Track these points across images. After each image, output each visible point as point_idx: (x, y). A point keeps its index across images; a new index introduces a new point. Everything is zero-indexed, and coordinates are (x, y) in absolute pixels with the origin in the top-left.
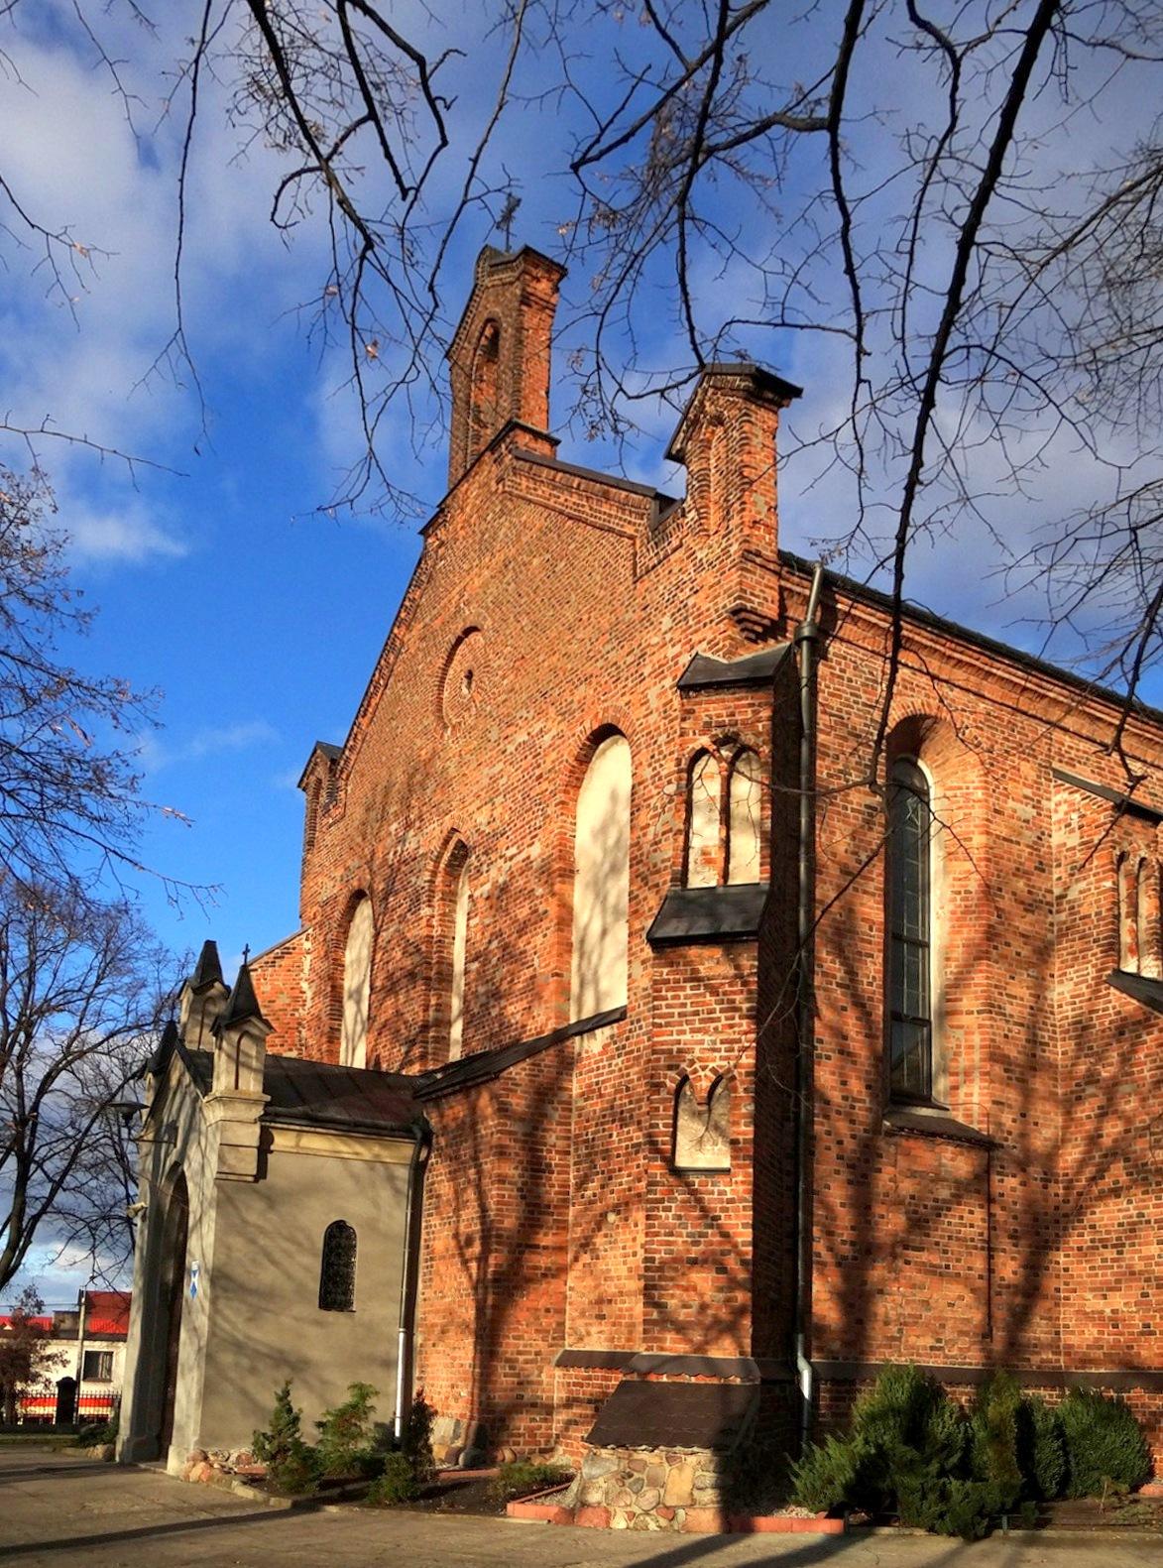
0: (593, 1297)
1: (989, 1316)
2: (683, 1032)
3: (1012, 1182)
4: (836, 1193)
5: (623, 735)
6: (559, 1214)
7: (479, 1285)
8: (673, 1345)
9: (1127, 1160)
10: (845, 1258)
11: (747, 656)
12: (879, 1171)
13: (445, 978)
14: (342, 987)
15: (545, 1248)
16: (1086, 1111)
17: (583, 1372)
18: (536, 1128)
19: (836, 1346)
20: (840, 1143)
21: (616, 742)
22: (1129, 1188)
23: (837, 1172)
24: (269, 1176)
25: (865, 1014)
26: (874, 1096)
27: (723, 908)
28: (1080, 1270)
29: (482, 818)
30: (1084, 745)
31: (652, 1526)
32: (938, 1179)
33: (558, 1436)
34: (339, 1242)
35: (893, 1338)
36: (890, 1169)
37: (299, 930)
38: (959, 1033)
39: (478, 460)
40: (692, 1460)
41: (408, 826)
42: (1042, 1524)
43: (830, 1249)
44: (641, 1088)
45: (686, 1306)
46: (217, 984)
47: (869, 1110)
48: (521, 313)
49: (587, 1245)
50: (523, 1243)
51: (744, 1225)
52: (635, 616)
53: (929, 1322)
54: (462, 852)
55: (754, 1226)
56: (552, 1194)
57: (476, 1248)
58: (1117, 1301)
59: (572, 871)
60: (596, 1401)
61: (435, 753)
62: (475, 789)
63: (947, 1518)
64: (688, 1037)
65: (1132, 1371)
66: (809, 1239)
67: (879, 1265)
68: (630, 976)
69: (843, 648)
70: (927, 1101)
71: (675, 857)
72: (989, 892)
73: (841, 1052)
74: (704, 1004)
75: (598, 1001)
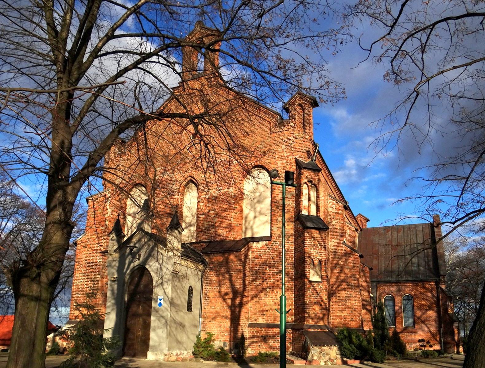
2: (311, 249)
16: (336, 271)
17: (259, 329)
44: (277, 259)
51: (326, 295)
57: (231, 296)
58: (345, 313)
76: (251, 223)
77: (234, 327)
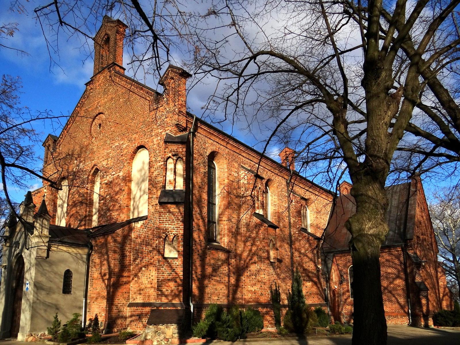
0: (138, 289)
1: (229, 291)
2: (167, 225)
3: (233, 260)
4: (198, 263)
5: (146, 148)
6: (129, 268)
7: (108, 286)
8: (164, 300)
9: (257, 256)
10: (199, 278)
11: (179, 135)
12: (206, 258)
13: (91, 203)
14: (57, 203)
15: (125, 276)
16: (249, 244)
17: (135, 308)
18: (123, 246)
19: (197, 300)
20: (198, 251)
21: (144, 150)
22: (258, 262)
23: (198, 258)
24: (50, 258)
25: (204, 221)
26: (205, 240)
27: (175, 195)
28: (248, 281)
29: (104, 163)
30: (247, 160)
31: (163, 343)
32: (218, 260)
33: (128, 325)
34: (68, 275)
35: (209, 297)
36: (209, 257)
37: (42, 186)
38: (222, 225)
39: (103, 70)
40: (172, 327)
41: (80, 162)
42: (246, 338)
43: (196, 276)
45: (167, 290)
46: (32, 204)
47: (204, 243)
48: (116, 35)
49: (136, 276)
50: (120, 275)
51: (181, 271)
52: (150, 120)
53: (216, 293)
54: (97, 170)
55: (183, 271)
56: (127, 262)
57: (107, 277)
59: (131, 180)
60: (139, 315)
61: (89, 144)
62: (102, 155)
63: (228, 337)
64: (167, 226)
65: (259, 304)
66: (192, 274)
67: (206, 280)
68: (148, 209)
69: (199, 135)
70: (215, 241)
71: (163, 182)
72: (229, 193)
73: (199, 230)
74: (171, 218)
75: (138, 214)
76: (138, 203)
77: (109, 307)
